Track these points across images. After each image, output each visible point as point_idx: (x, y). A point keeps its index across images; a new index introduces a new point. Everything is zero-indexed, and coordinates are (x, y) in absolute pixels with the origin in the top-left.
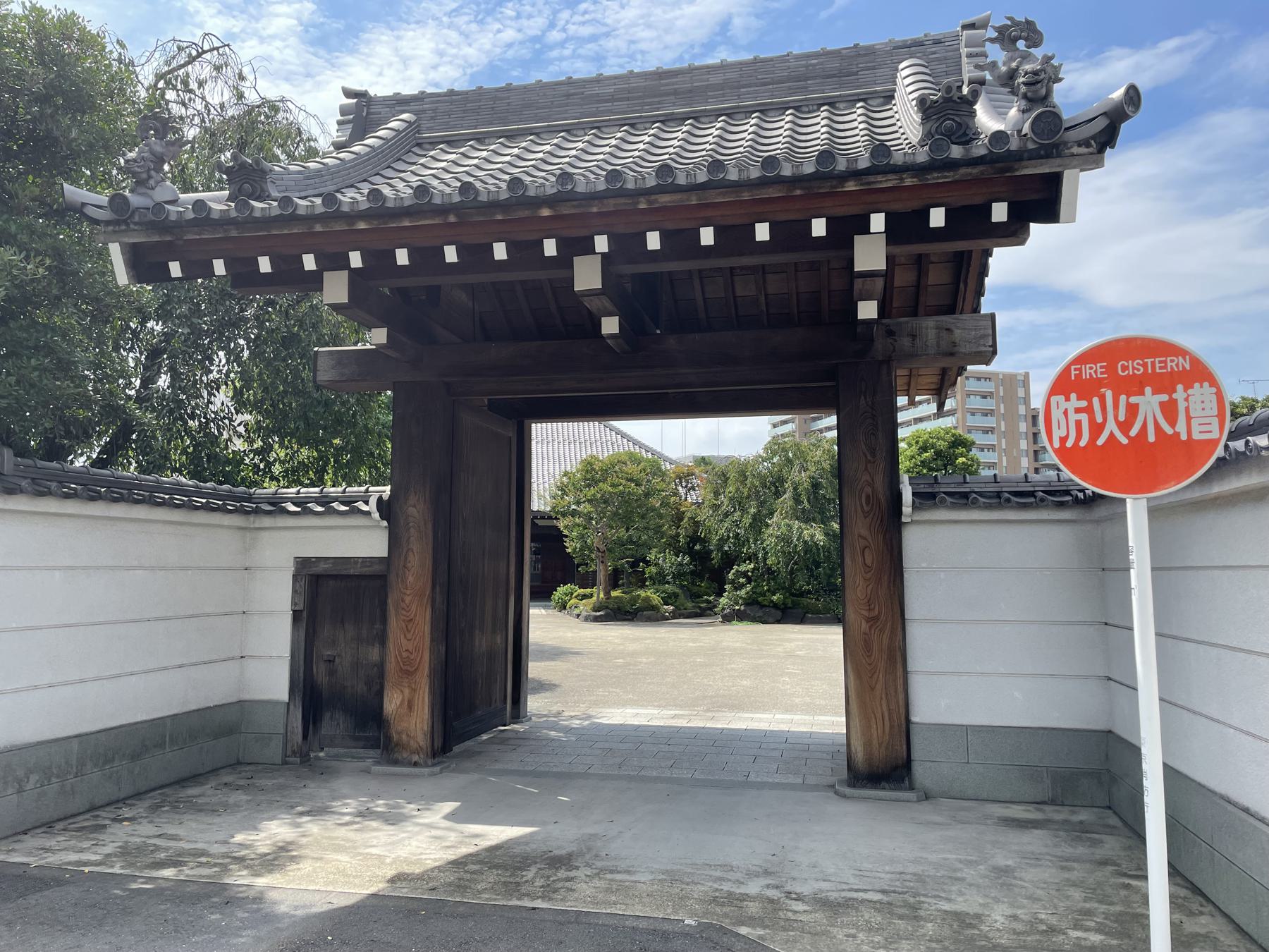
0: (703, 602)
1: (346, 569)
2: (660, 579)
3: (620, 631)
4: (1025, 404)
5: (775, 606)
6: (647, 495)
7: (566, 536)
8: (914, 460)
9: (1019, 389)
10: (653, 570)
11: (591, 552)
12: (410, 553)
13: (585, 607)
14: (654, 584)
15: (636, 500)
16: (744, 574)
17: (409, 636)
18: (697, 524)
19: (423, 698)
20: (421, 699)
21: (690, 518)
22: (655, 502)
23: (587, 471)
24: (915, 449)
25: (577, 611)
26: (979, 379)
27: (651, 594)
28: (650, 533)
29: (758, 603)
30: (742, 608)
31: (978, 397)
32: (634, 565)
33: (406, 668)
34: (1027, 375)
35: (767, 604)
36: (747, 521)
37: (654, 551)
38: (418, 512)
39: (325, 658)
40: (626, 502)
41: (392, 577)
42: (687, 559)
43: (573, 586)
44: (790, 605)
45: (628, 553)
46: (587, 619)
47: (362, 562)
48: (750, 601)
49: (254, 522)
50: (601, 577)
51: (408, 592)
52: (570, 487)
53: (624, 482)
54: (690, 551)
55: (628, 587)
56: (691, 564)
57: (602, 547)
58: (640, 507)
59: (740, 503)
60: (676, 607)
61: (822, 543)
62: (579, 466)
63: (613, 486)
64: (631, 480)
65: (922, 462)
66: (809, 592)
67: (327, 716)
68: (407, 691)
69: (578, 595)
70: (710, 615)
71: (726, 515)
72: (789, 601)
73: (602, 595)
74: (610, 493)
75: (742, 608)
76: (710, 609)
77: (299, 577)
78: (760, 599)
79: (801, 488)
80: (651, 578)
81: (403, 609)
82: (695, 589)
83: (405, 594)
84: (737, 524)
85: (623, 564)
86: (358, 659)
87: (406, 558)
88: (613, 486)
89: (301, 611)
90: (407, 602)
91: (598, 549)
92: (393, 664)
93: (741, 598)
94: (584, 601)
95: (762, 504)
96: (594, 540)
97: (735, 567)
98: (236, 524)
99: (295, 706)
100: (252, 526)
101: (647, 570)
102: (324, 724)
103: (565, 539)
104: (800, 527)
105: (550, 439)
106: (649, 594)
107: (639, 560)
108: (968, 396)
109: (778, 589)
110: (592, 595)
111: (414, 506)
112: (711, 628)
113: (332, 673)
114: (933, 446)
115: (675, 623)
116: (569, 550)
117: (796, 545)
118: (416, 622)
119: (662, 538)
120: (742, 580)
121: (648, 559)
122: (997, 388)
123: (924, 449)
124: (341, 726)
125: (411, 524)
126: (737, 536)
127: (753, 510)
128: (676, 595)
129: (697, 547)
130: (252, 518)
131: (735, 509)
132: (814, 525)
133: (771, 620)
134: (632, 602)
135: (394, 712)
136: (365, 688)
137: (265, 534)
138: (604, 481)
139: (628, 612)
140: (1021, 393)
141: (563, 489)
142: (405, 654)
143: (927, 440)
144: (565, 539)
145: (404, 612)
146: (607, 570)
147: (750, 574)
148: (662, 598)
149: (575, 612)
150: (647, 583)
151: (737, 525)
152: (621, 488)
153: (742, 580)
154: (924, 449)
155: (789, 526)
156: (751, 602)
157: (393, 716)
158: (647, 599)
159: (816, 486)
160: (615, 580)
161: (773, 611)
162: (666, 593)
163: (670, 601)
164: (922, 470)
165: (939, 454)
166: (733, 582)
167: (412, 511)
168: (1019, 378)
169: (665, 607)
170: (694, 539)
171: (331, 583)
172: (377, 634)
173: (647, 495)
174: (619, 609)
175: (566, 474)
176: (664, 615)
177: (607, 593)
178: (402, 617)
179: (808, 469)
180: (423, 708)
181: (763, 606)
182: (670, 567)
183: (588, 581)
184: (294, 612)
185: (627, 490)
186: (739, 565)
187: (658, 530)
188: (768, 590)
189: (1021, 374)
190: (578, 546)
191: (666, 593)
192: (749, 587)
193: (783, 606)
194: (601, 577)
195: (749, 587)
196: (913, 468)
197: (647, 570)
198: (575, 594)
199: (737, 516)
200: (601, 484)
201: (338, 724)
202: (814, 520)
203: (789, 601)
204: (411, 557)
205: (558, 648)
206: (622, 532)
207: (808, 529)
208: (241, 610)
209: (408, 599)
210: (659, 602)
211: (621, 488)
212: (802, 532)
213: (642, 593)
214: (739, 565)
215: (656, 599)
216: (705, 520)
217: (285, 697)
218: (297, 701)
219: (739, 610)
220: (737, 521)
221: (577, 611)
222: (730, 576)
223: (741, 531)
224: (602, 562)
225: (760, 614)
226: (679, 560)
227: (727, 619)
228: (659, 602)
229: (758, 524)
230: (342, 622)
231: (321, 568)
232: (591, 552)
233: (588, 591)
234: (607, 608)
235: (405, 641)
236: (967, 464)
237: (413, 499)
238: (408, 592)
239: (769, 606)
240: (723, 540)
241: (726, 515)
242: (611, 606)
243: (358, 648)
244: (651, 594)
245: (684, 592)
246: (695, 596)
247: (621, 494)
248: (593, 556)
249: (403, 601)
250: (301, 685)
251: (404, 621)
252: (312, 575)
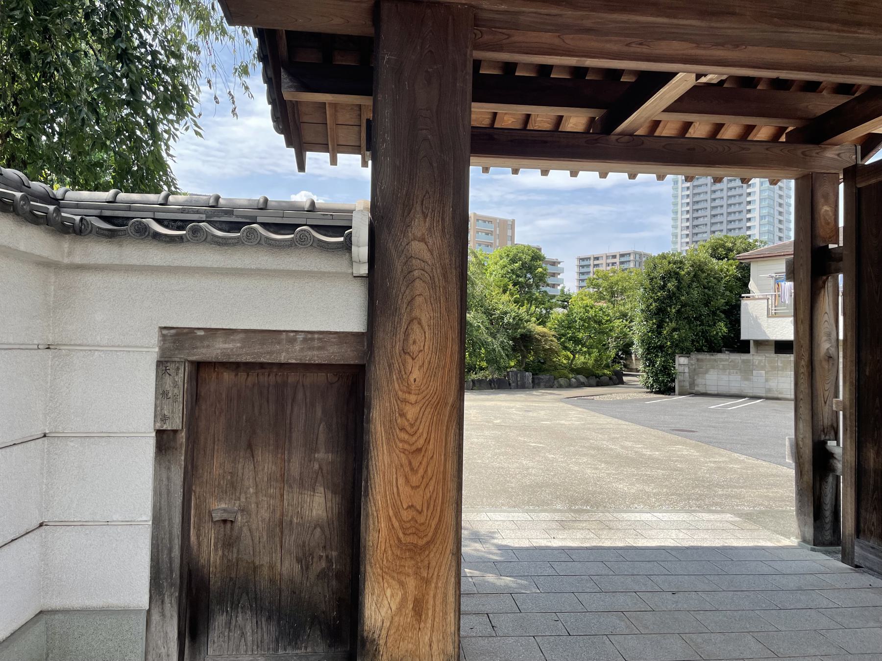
1: (270, 353)
4: (511, 240)
9: (508, 230)
12: (415, 326)
17: (415, 480)
19: (445, 595)
20: (439, 596)
26: (485, 221)
31: (484, 234)
33: (409, 539)
34: (513, 221)
38: (431, 251)
39: (217, 516)
41: (379, 373)
47: (305, 340)
49: (70, 254)
51: (412, 398)
65: (512, 270)
67: (219, 621)
68: (411, 583)
77: (172, 367)
81: (402, 429)
83: (405, 401)
86: (282, 515)
87: (407, 334)
89: (175, 432)
90: (410, 416)
92: (384, 532)
98: (37, 252)
99: (163, 615)
100: (66, 261)
102: (214, 635)
111: (422, 240)
113: (229, 543)
114: (520, 259)
118: (429, 454)
122: (495, 229)
124: (250, 639)
125: (416, 273)
130: (66, 243)
135: (387, 624)
136: (297, 567)
137: (93, 280)
140: (509, 233)
142: (406, 515)
145: (403, 435)
154: (513, 261)
157: (384, 632)
167: (417, 247)
171: (227, 377)
172: (321, 468)
178: (400, 445)
180: (445, 613)
184: (159, 433)
189: (509, 220)
196: (505, 274)
201: (243, 634)
204: (416, 333)
208: (39, 434)
209: (411, 412)
217: (140, 597)
218: (168, 606)
230: (250, 447)
231: (217, 350)
235: (408, 489)
237: (419, 226)
238: (412, 398)
243: (282, 495)
249: (403, 415)
250: (176, 575)
251: (404, 451)
252: (192, 363)
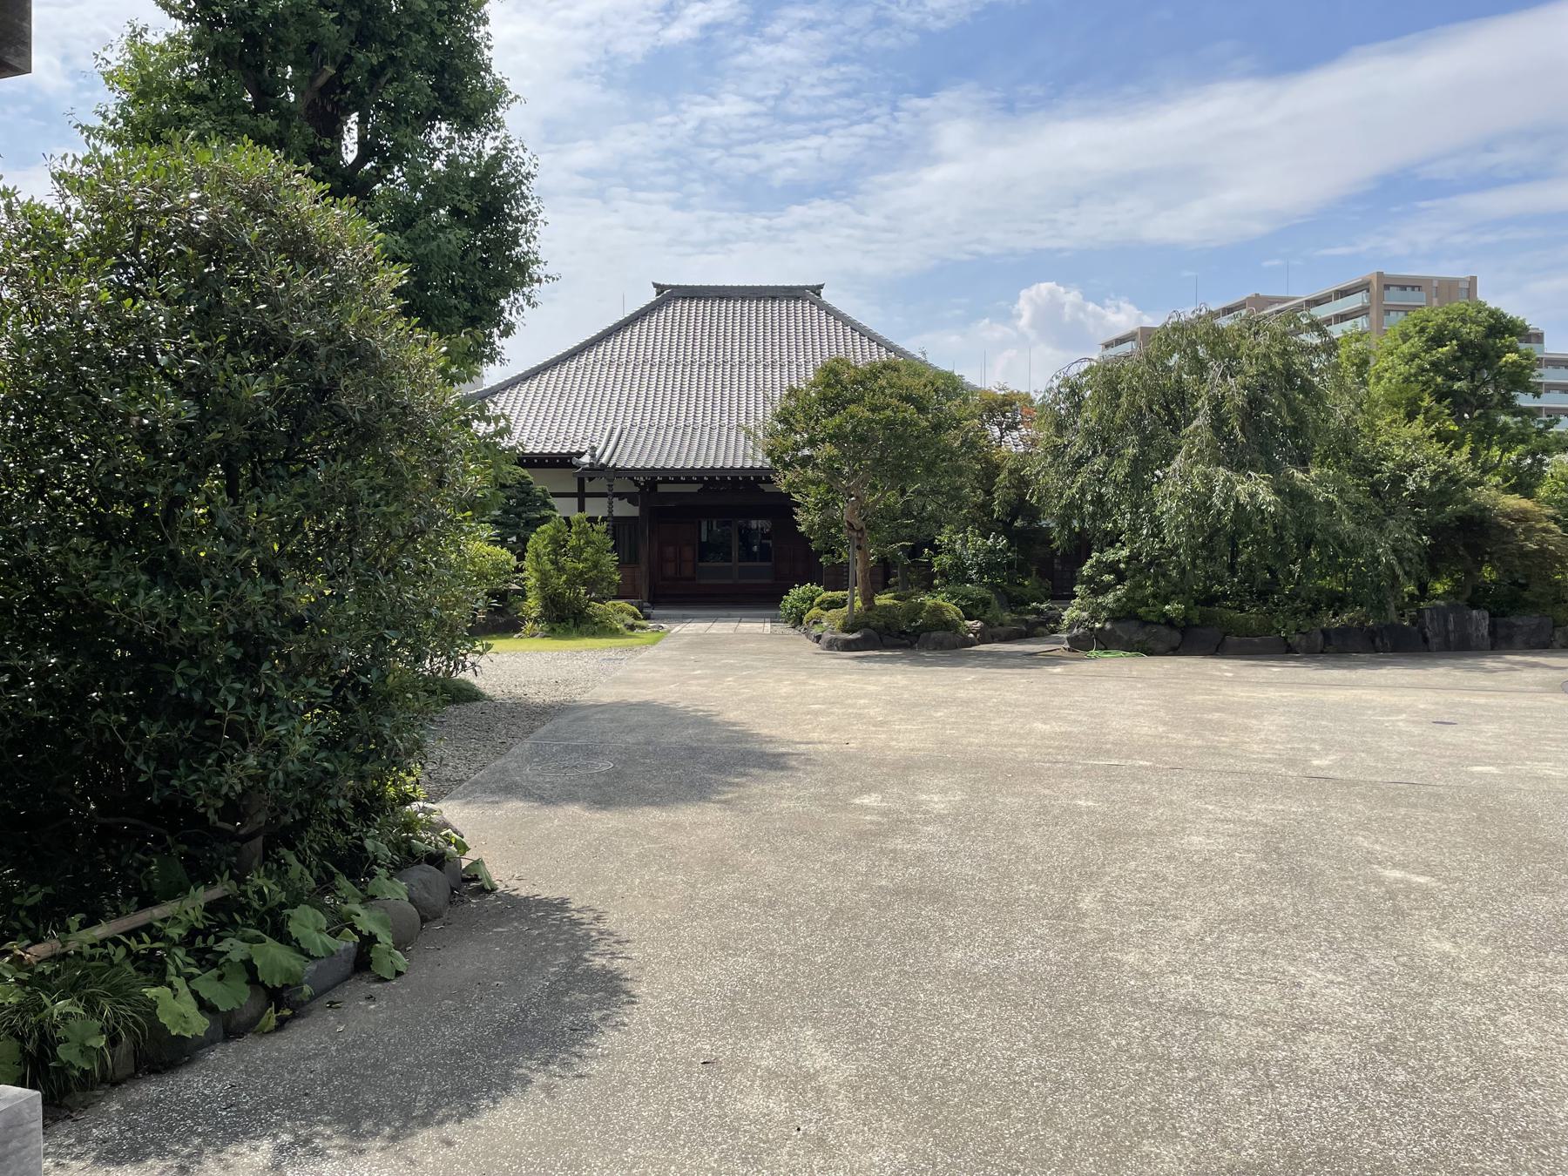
0: (1029, 612)
2: (958, 574)
3: (885, 679)
5: (1170, 622)
6: (937, 427)
7: (798, 505)
8: (1417, 361)
10: (946, 559)
11: (840, 531)
13: (831, 622)
14: (948, 582)
15: (917, 437)
16: (1112, 567)
18: (1023, 483)
21: (1011, 472)
22: (952, 438)
23: (828, 385)
24: (1417, 342)
25: (816, 630)
26: (1404, 288)
27: (940, 601)
28: (941, 499)
29: (1136, 617)
30: (1108, 626)
32: (914, 552)
35: (1155, 619)
36: (1120, 472)
37: (947, 530)
40: (898, 437)
42: (1003, 542)
43: (815, 587)
44: (1197, 621)
45: (904, 532)
46: (832, 645)
48: (1123, 614)
50: (857, 570)
52: (800, 416)
53: (895, 402)
54: (1006, 529)
55: (905, 588)
56: (1009, 550)
57: (858, 522)
58: (925, 447)
59: (1105, 441)
60: (986, 622)
61: (1272, 509)
62: (811, 376)
63: (874, 409)
64: (908, 399)
65: (1433, 364)
66: (1225, 596)
69: (823, 602)
70: (1043, 635)
71: (1079, 462)
72: (1195, 615)
73: (859, 604)
74: (870, 421)
75: (1108, 626)
76: (1043, 624)
78: (1142, 611)
79: (1227, 406)
80: (943, 573)
82: (1016, 591)
84: (1101, 478)
85: (893, 553)
88: (874, 409)
91: (850, 524)
93: (1104, 608)
94: (832, 611)
95: (1146, 441)
96: (844, 511)
97: (1095, 555)
101: (936, 561)
103: (795, 509)
104: (1228, 479)
105: (785, 360)
106: (940, 602)
107: (922, 545)
108: (1388, 312)
109: (1173, 593)
110: (844, 601)
112: (1058, 670)
114: (1455, 335)
115: (990, 654)
116: (802, 529)
117: (1220, 513)
119: (960, 508)
120: (1107, 578)
121: (937, 542)
123: (1438, 340)
126: (1099, 500)
127: (1131, 451)
128: (986, 603)
129: (1018, 523)
131: (1095, 452)
132: (1252, 474)
133: (1160, 647)
134: (911, 615)
138: (857, 400)
139: (904, 632)
141: (785, 417)
143: (1444, 324)
144: (795, 509)
146: (866, 562)
147: (1122, 566)
148: (962, 608)
149: (813, 631)
150: (936, 582)
151: (1100, 480)
152: (889, 412)
153: (1107, 578)
154: (1438, 340)
155: (1206, 476)
156: (1124, 615)
158: (937, 609)
159: (1255, 402)
160: (882, 576)
161: (1164, 631)
162: (970, 599)
163: (976, 613)
164: (1433, 379)
165: (1465, 347)
166: (1091, 579)
168: (1461, 285)
169: (968, 623)
170: (1019, 507)
173: (937, 427)
174: (887, 627)
175: (792, 393)
176: (966, 638)
177: (868, 600)
179: (1241, 371)
181: (1145, 623)
182: (974, 555)
183: (837, 578)
185: (900, 415)
186: (1101, 551)
187: (955, 495)
188: (1155, 596)
190: (817, 520)
191: (970, 599)
192: (1121, 590)
193: (1183, 623)
194: (857, 570)
195: (1121, 590)
196: (1415, 375)
197: (936, 561)
198: (818, 600)
199: (1098, 463)
200: (853, 408)
202: (1253, 467)
203: (1195, 615)
205: (745, 736)
206: (892, 497)
207: (1242, 483)
210: (958, 615)
211: (889, 412)
212: (1233, 489)
213: (928, 600)
214: (1101, 551)
215: (952, 610)
216: (1038, 473)
219: (1101, 629)
220: (1099, 472)
221: (816, 630)
222: (1086, 570)
223: (1108, 491)
224: (859, 548)
225: (1140, 636)
226: (989, 543)
227: (1082, 644)
228: (958, 615)
229: (1139, 480)
232: (840, 531)
233: (839, 594)
234: (867, 625)
236: (1520, 365)
239: (1158, 623)
240: (1073, 507)
241: (1079, 462)
242: (874, 623)
244: (940, 601)
245: (997, 598)
246: (1015, 602)
247: (889, 424)
248: (842, 536)
